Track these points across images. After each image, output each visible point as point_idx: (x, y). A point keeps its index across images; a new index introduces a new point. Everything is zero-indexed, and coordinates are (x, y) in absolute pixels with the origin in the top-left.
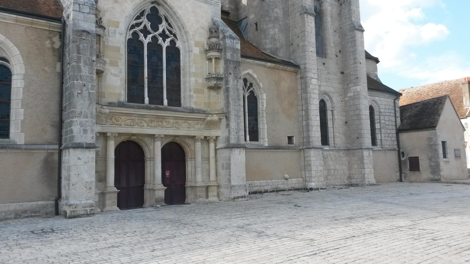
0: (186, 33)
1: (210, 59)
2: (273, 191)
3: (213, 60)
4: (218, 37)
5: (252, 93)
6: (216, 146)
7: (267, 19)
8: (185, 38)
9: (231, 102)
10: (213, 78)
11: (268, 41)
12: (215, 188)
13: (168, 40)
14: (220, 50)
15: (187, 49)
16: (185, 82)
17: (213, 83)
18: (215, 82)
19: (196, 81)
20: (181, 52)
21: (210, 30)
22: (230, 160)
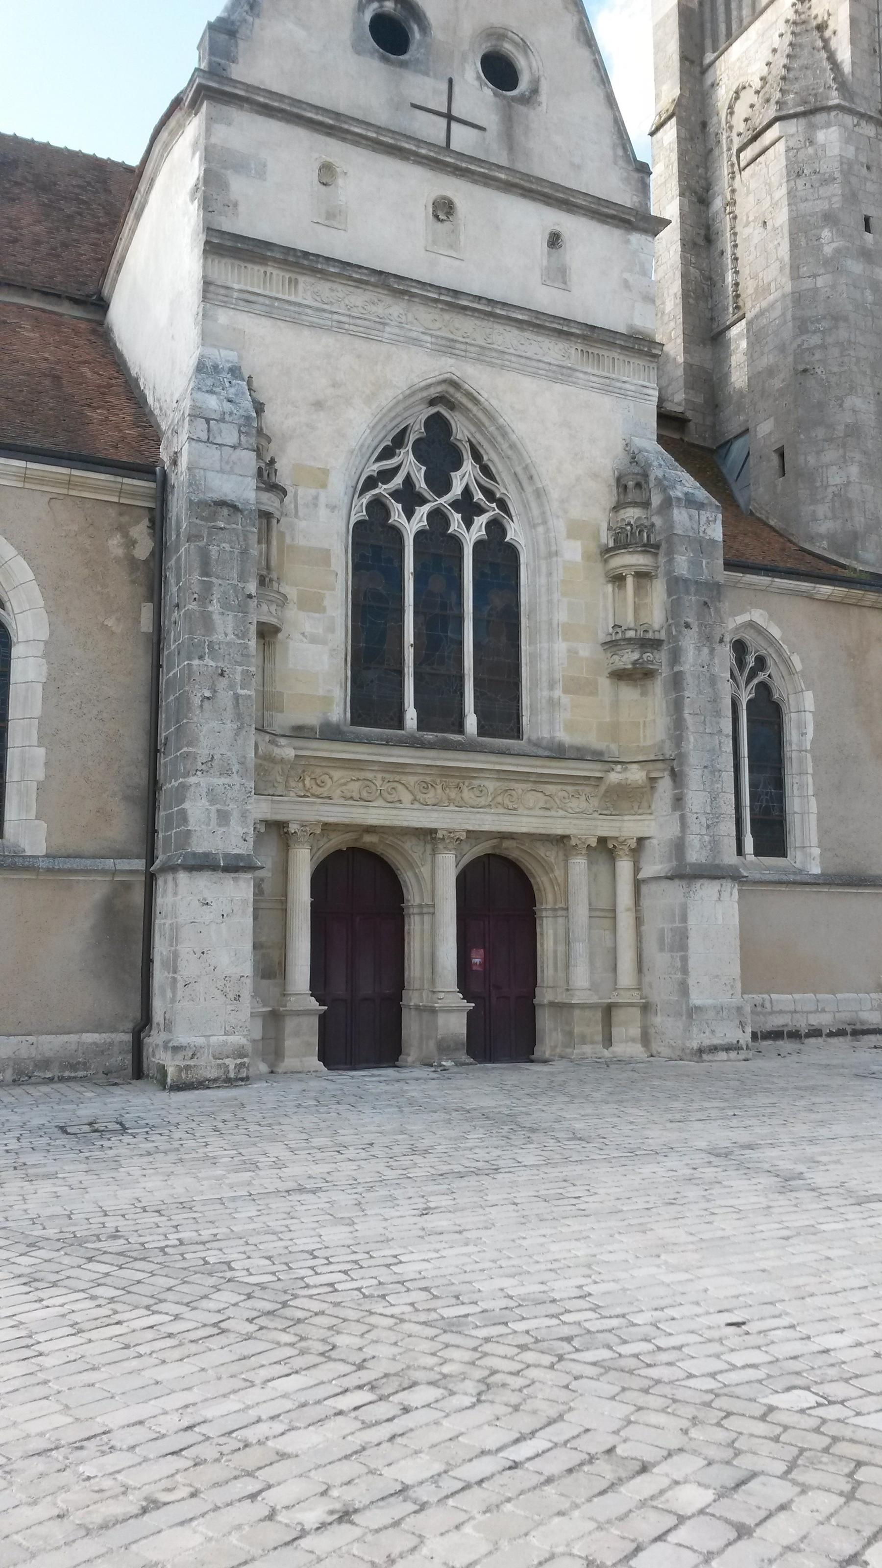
0: (540, 494)
1: (618, 579)
2: (841, 1033)
3: (630, 581)
4: (646, 504)
5: (764, 689)
6: (637, 870)
7: (820, 433)
8: (536, 512)
9: (689, 719)
10: (630, 640)
11: (822, 510)
12: (636, 1012)
13: (481, 521)
14: (651, 548)
15: (542, 547)
16: (533, 657)
17: (628, 658)
18: (636, 656)
19: (572, 653)
20: (523, 559)
21: (618, 480)
22: (684, 918)
